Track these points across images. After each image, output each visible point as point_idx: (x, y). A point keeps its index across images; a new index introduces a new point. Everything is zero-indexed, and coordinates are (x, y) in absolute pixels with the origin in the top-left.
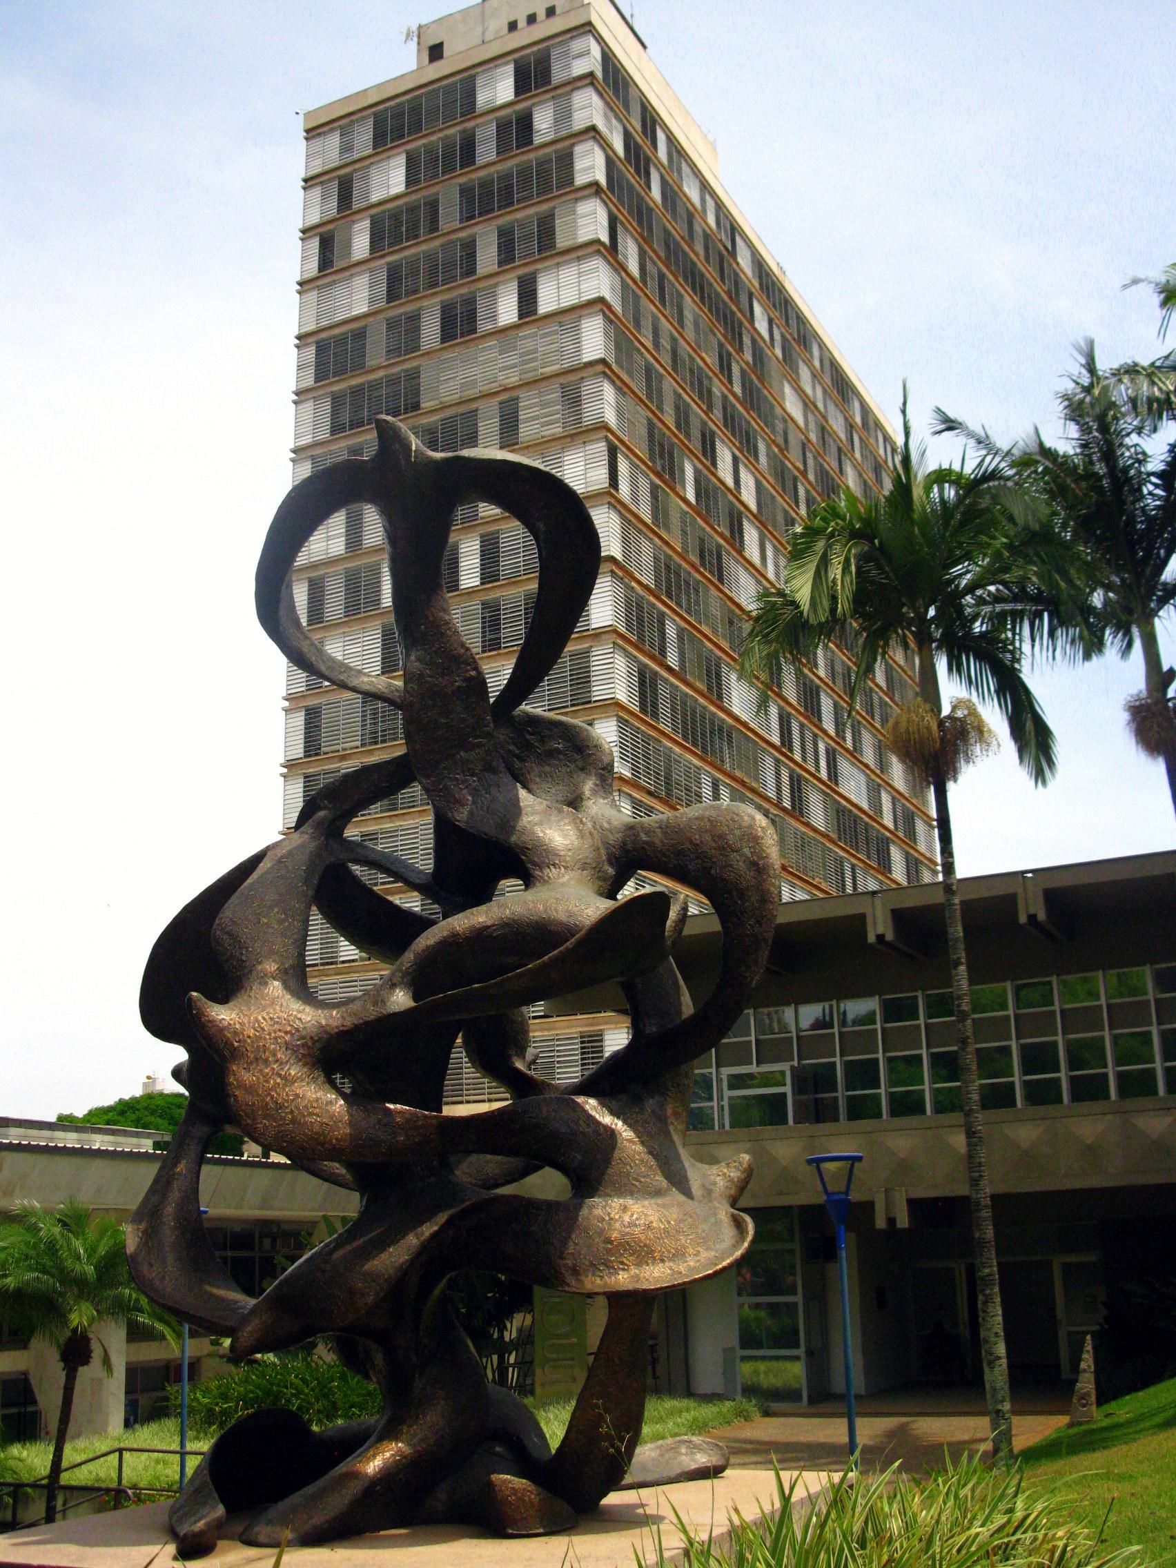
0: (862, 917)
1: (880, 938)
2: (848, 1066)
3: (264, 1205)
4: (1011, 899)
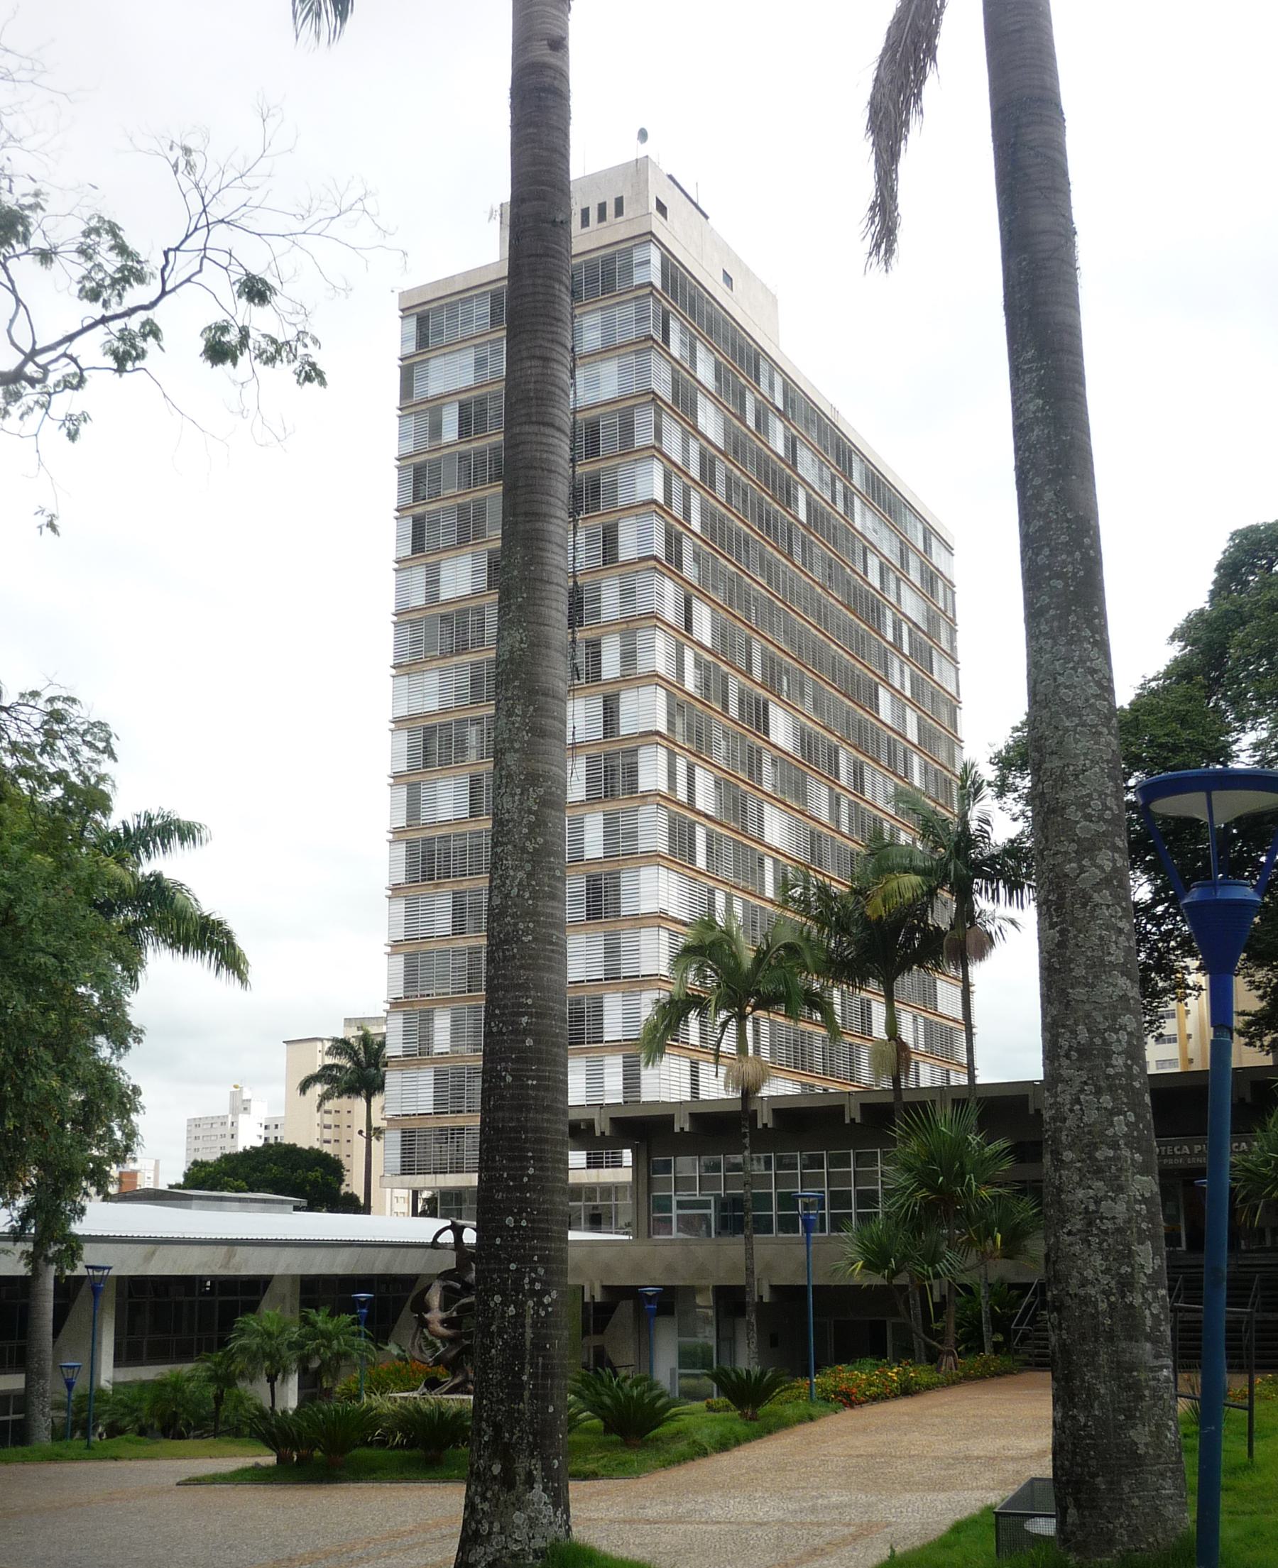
0: (843, 1106)
1: (765, 1125)
2: (780, 1195)
3: (226, 1266)
4: (841, 1109)
